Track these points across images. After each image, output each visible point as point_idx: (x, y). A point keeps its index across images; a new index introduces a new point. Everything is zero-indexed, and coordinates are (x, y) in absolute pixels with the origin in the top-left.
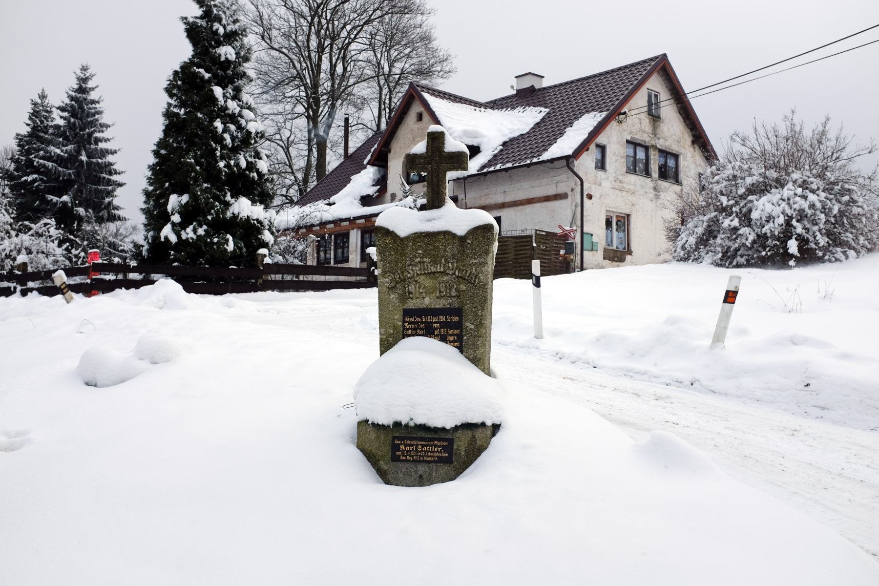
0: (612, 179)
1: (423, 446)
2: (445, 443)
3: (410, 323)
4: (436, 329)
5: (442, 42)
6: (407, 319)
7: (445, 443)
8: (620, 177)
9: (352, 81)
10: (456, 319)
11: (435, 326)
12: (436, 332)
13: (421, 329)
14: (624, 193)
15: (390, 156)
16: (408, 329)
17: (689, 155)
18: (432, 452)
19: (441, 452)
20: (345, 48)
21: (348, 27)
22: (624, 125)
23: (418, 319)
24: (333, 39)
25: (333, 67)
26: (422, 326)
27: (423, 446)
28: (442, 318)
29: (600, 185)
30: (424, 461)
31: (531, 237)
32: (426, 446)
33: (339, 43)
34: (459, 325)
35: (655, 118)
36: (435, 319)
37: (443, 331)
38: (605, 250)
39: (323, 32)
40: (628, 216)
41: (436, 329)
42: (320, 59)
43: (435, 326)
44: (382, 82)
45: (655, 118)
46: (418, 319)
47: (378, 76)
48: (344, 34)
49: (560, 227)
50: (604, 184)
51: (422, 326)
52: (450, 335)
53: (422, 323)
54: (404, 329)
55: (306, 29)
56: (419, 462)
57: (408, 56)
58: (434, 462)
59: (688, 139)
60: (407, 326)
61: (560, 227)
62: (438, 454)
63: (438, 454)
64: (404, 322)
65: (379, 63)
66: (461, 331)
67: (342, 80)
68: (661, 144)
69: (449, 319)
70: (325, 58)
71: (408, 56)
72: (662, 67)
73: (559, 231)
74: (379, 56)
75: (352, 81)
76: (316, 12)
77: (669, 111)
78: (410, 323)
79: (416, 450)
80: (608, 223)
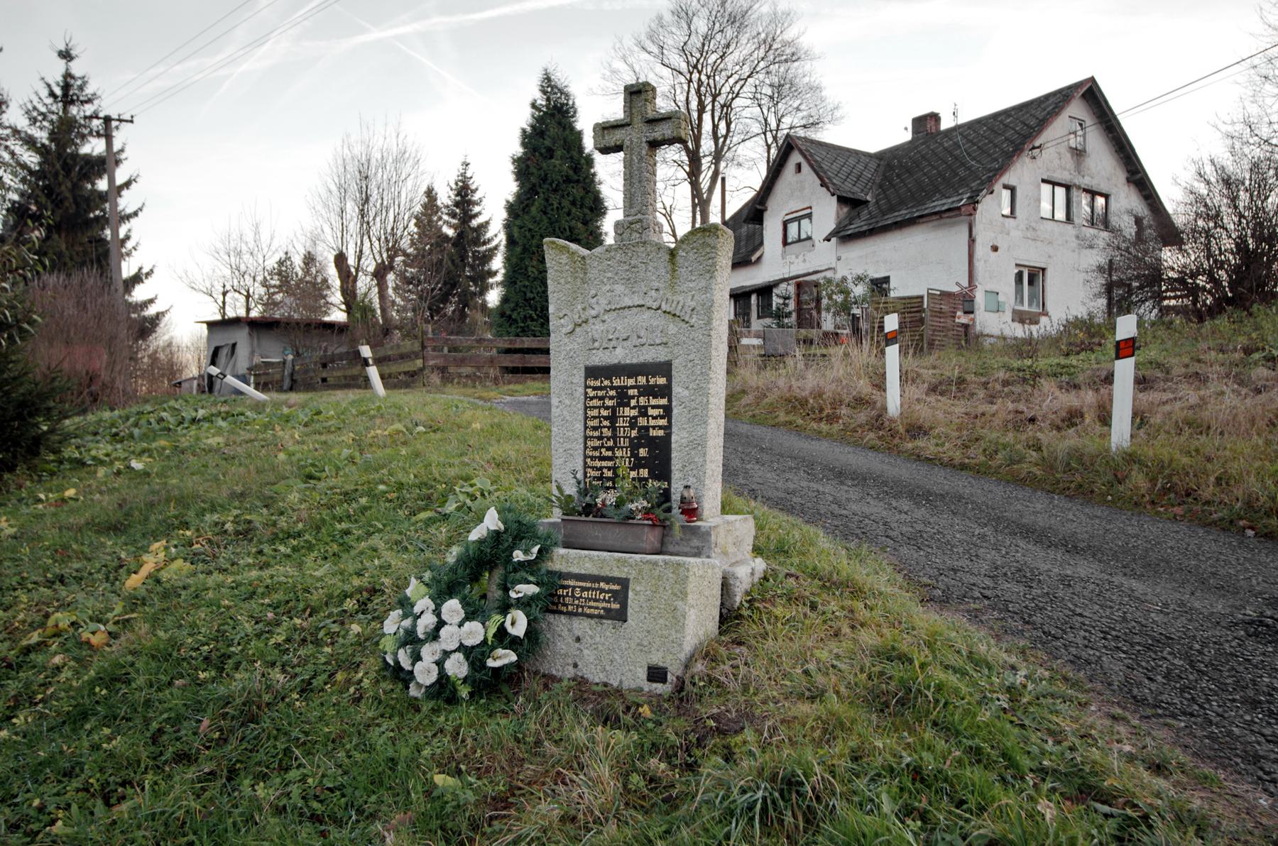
0: (1022, 226)
1: (583, 589)
2: (616, 587)
3: (595, 389)
4: (633, 397)
5: (831, 94)
6: (592, 383)
7: (616, 587)
8: (1033, 224)
9: (735, 140)
10: (662, 381)
11: (631, 392)
12: (633, 402)
13: (611, 398)
14: (1039, 243)
15: (767, 216)
16: (592, 399)
17: (1123, 195)
18: (596, 600)
19: (609, 602)
20: (727, 106)
21: (731, 81)
22: (1039, 162)
23: (606, 383)
24: (715, 97)
25: (715, 127)
26: (613, 393)
27: (583, 589)
28: (642, 380)
29: (1008, 234)
30: (583, 614)
31: (922, 297)
32: (587, 589)
33: (721, 99)
34: (666, 391)
35: (1079, 154)
36: (631, 382)
37: (642, 401)
38: (1014, 312)
39: (703, 89)
40: (1044, 270)
41: (633, 397)
42: (700, 118)
43: (631, 392)
44: (770, 140)
45: (1079, 154)
46: (606, 383)
47: (765, 133)
48: (726, 89)
49: (957, 284)
50: (1014, 233)
51: (613, 393)
52: (654, 407)
53: (612, 388)
54: (586, 398)
55: (686, 87)
56: (576, 614)
57: (798, 109)
58: (600, 617)
59: (1121, 176)
60: (591, 393)
61: (957, 284)
62: (604, 605)
63: (604, 605)
64: (586, 387)
65: (766, 120)
66: (670, 401)
67: (725, 137)
68: (1086, 181)
69: (652, 381)
70: (707, 117)
71: (798, 109)
72: (1091, 94)
73: (956, 289)
74: (765, 111)
75: (735, 140)
76: (695, 67)
77: (1096, 143)
78: (595, 389)
79: (573, 596)
80: (1019, 276)
